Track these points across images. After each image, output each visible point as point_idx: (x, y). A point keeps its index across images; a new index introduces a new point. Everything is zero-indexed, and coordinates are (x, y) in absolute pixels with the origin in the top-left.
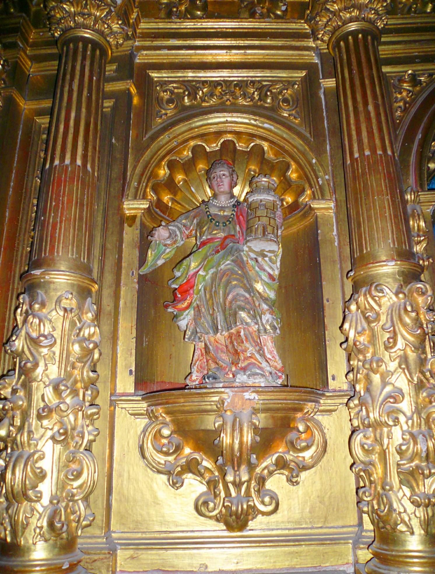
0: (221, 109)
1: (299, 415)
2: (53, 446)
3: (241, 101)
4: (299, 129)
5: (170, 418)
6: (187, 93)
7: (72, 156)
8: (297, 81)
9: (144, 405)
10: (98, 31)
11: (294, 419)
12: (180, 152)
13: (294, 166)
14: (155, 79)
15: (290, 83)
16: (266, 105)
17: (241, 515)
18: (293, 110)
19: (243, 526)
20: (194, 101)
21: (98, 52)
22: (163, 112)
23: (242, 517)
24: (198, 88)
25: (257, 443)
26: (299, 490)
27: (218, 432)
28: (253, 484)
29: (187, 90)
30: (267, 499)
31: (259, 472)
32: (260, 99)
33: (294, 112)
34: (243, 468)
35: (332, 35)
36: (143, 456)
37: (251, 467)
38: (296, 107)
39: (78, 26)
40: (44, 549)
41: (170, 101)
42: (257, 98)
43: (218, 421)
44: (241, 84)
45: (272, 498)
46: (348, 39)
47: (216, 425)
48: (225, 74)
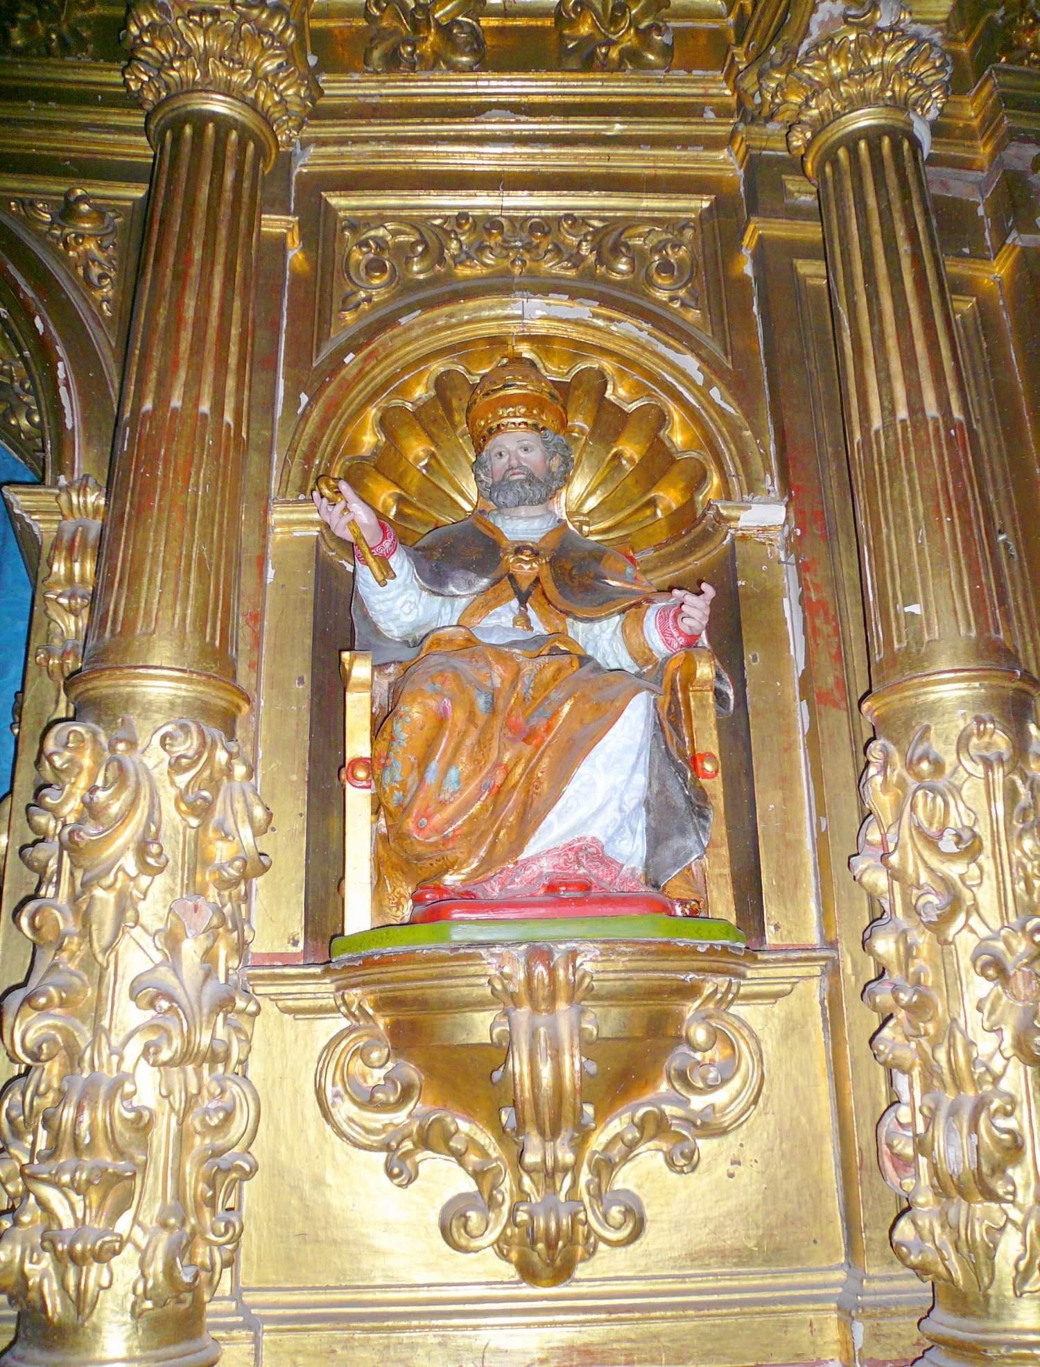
0: (501, 285)
1: (690, 1008)
2: (138, 1059)
3: (551, 266)
4: (694, 332)
5: (388, 1020)
6: (420, 249)
7: (215, 378)
8: (689, 220)
9: (327, 986)
10: (253, 105)
11: (679, 1019)
12: (403, 391)
13: (676, 415)
14: (341, 214)
15: (673, 225)
16: (618, 277)
17: (558, 1239)
18: (680, 288)
19: (563, 1272)
20: (437, 267)
21: (251, 146)
22: (362, 294)
23: (560, 1244)
24: (447, 233)
25: (591, 1076)
26: (696, 1182)
27: (502, 1049)
28: (585, 1175)
29: (422, 241)
30: (616, 1213)
31: (600, 1148)
32: (600, 260)
33: (682, 293)
34: (565, 1135)
35: (814, 136)
36: (326, 1114)
37: (583, 1134)
38: (689, 280)
39: (189, 88)
40: (79, 1344)
41: (376, 266)
42: (592, 258)
43: (500, 1024)
44: (546, 226)
45: (628, 1212)
46: (857, 144)
47: (497, 1030)
48: (482, 201)
